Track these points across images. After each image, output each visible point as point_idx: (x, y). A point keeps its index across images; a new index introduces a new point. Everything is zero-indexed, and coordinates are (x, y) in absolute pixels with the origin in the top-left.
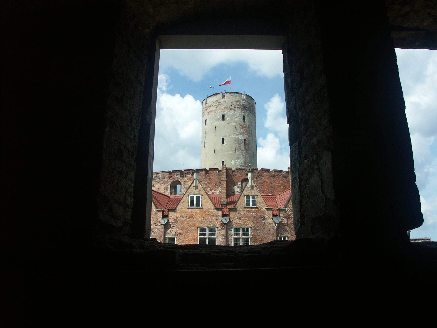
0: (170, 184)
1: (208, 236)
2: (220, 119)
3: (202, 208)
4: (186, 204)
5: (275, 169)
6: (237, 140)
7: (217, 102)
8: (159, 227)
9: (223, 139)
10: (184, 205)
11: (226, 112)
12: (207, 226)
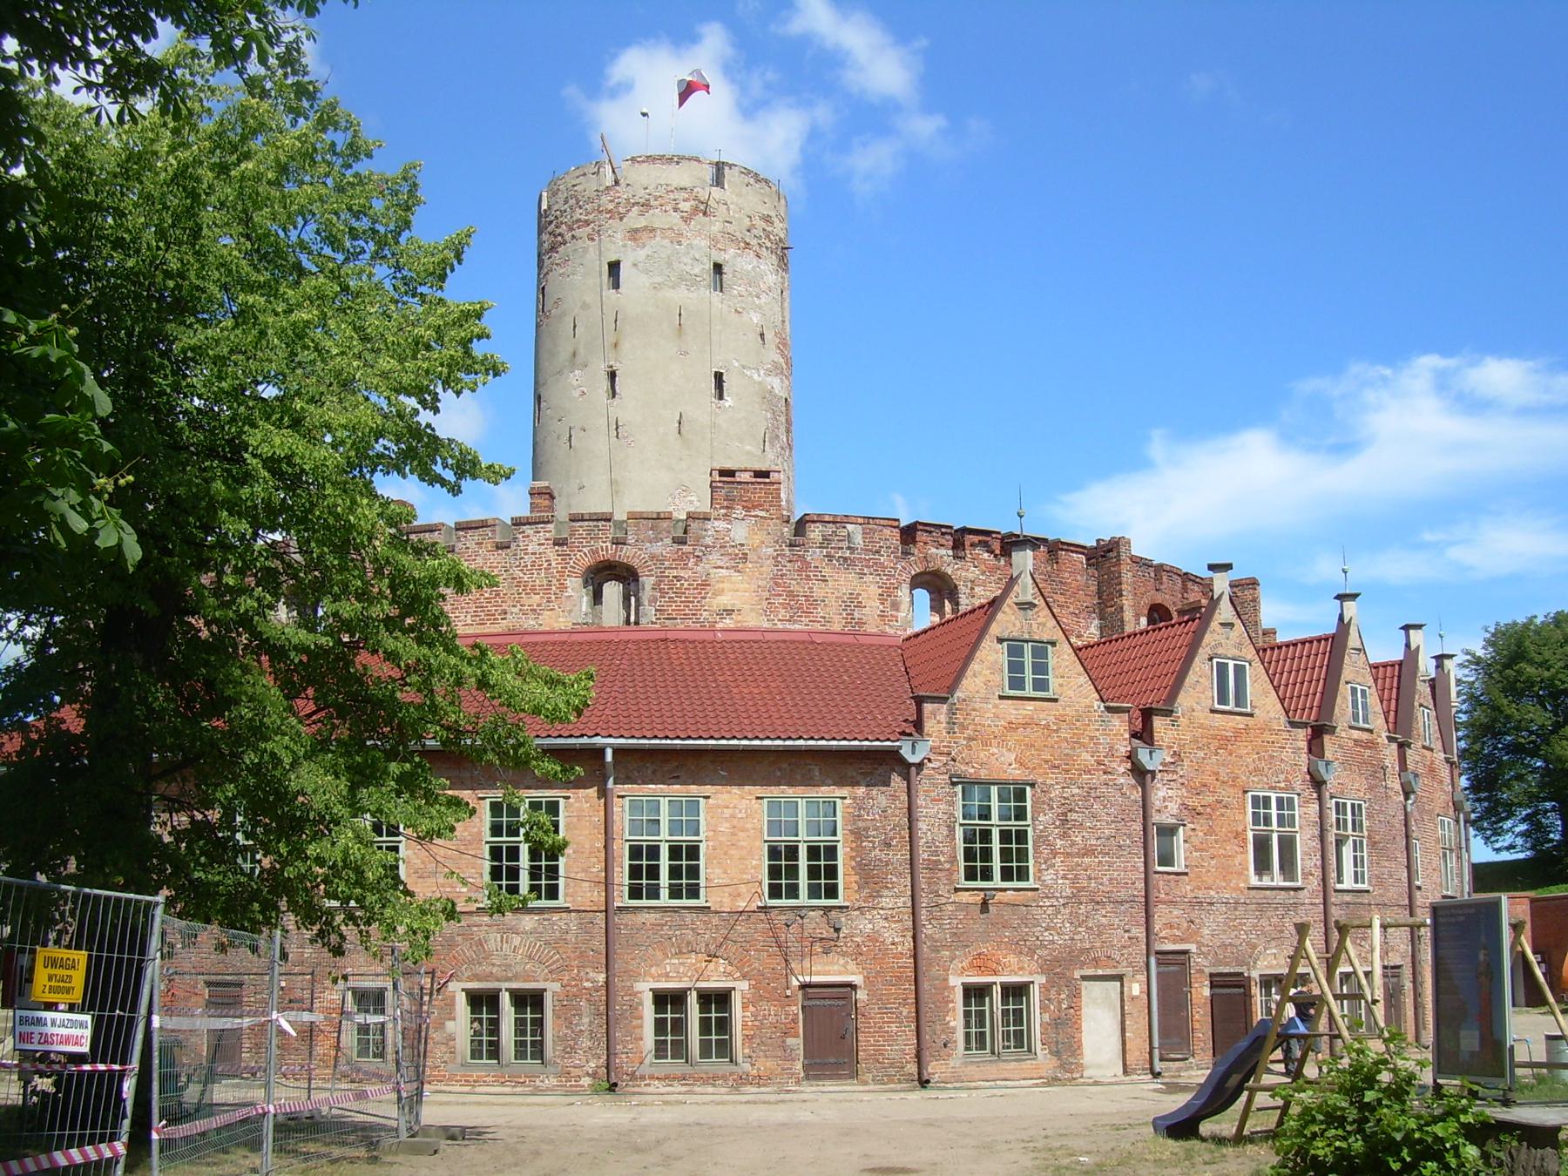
3: (1251, 715)
6: (767, 397)
8: (1122, 781)
9: (719, 377)
10: (1198, 697)
11: (728, 256)
12: (1274, 788)
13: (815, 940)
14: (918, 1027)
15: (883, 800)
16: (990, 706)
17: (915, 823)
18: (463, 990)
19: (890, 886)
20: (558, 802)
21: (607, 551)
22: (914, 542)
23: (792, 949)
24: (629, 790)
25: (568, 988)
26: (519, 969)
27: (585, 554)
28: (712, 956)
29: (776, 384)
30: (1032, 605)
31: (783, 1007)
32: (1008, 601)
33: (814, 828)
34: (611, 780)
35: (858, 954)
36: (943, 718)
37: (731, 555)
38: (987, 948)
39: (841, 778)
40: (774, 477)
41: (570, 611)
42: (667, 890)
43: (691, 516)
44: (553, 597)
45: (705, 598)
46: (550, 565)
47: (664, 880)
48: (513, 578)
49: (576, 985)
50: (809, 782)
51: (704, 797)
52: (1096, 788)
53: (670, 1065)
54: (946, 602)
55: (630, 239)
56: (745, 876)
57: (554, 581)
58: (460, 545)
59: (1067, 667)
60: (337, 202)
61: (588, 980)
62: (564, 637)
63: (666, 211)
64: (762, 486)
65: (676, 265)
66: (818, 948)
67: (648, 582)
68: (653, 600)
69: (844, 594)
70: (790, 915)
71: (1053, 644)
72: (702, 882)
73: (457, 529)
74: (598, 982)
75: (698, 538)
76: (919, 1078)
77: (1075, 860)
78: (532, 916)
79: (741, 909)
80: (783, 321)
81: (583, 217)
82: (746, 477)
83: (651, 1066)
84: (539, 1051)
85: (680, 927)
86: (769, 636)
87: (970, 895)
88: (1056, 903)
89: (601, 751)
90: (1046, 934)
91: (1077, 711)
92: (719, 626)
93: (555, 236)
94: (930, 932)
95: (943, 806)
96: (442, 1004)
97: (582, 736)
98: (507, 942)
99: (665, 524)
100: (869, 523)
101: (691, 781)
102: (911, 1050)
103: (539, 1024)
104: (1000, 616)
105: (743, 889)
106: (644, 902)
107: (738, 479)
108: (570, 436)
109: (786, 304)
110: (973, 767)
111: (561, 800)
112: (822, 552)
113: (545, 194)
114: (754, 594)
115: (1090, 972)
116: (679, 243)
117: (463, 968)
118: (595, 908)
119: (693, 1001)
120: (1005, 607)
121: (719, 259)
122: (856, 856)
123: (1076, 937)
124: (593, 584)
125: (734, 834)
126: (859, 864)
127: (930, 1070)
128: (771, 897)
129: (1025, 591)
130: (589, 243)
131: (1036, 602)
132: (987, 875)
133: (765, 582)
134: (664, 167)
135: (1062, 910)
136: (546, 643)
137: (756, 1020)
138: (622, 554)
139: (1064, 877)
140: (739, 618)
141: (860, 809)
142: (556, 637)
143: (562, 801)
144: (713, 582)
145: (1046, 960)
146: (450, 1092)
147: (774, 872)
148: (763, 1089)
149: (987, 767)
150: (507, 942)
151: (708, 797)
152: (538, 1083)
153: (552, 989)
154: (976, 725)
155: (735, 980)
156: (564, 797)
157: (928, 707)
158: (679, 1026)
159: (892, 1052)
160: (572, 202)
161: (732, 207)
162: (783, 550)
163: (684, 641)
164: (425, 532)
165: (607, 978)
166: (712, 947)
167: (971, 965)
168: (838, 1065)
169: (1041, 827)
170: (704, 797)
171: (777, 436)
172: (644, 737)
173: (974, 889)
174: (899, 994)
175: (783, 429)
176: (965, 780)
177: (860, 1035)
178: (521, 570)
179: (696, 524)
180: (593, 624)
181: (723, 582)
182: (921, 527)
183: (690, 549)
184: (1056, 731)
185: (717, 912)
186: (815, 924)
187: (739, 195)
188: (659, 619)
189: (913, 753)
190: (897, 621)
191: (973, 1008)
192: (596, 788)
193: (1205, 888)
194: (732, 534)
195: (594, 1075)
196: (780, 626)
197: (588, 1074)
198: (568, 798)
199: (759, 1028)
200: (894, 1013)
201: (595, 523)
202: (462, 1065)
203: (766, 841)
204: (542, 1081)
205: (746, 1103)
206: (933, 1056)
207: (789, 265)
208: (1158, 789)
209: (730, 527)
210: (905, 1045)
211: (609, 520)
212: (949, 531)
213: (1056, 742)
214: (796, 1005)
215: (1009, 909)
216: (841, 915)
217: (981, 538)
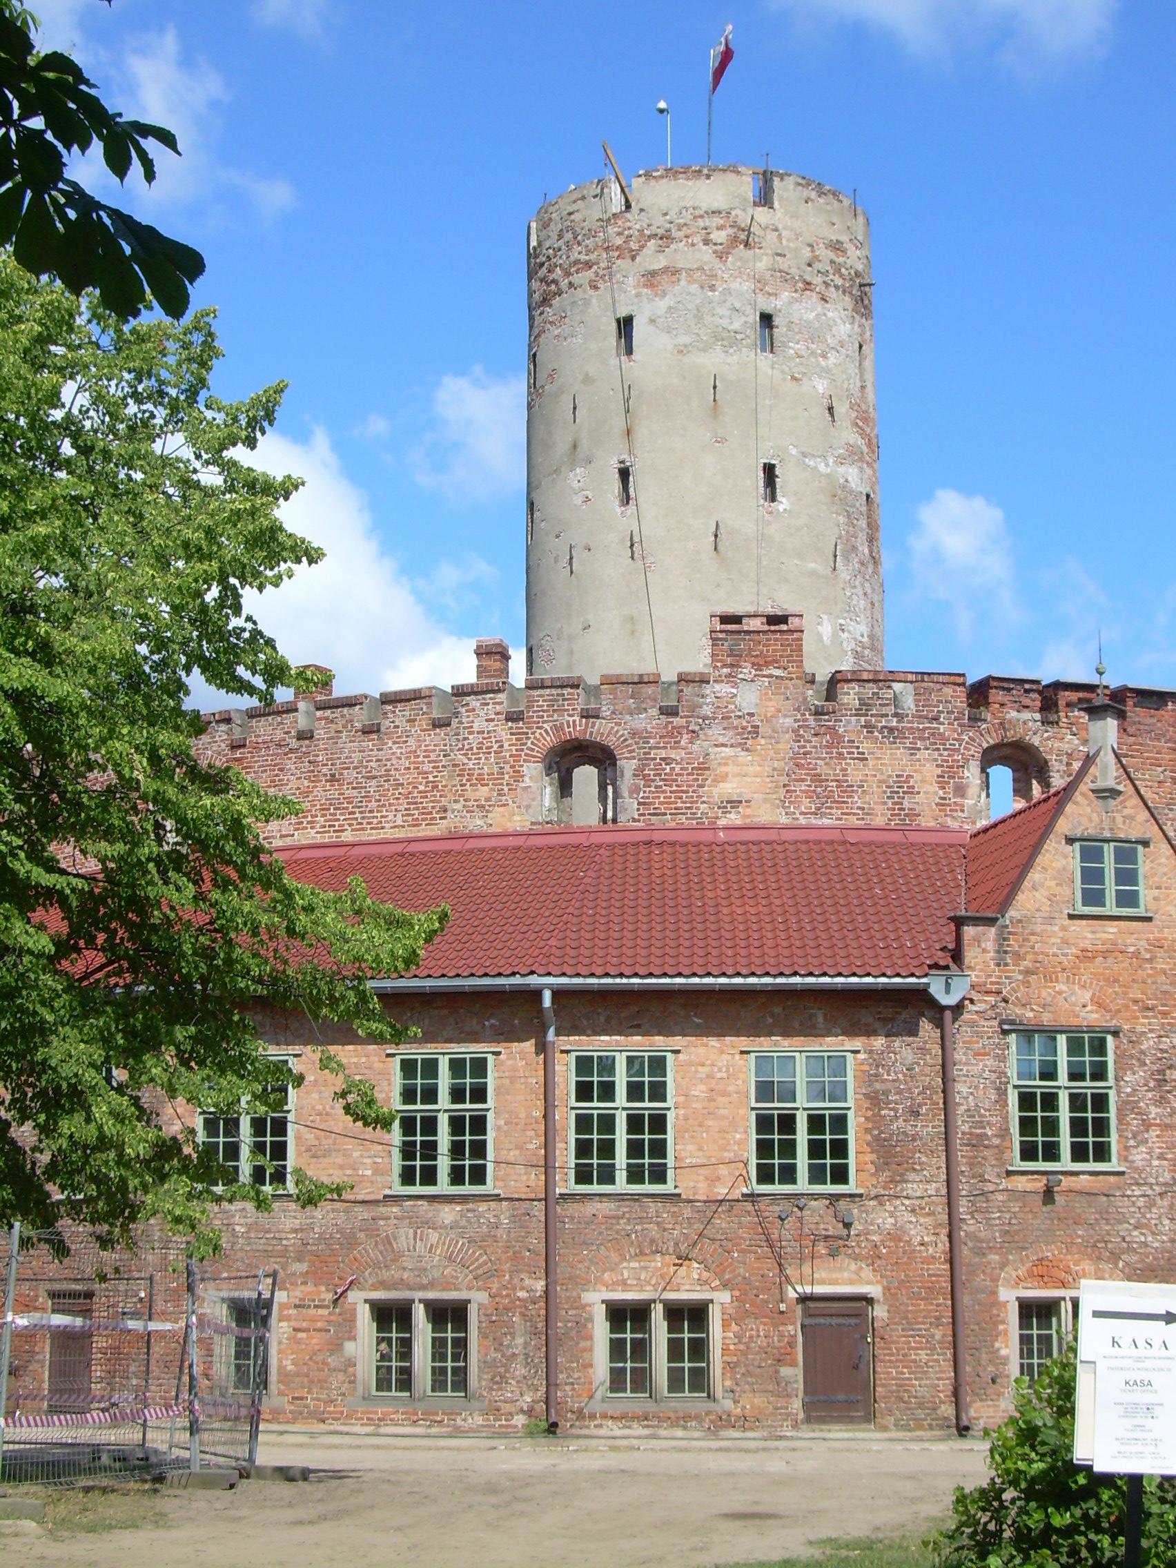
0: (978, 756)
6: (838, 494)
7: (721, 222)
9: (770, 472)
11: (781, 302)
13: (816, 1239)
14: (955, 1355)
15: (908, 1055)
16: (1056, 928)
17: (950, 1083)
18: (366, 1301)
19: (918, 1167)
20: (485, 1059)
21: (575, 727)
22: (987, 704)
23: (789, 1250)
24: (575, 1042)
25: (497, 1299)
28: (684, 1258)
29: (853, 476)
30: (1114, 793)
31: (775, 1325)
32: (1083, 788)
33: (818, 1092)
34: (552, 1031)
36: (990, 945)
37: (736, 728)
38: (1051, 1251)
40: (794, 623)
41: (528, 807)
42: (624, 1173)
43: (684, 679)
44: (506, 789)
45: (702, 786)
46: (502, 746)
47: (621, 1159)
48: (454, 765)
49: (508, 1295)
50: (809, 1030)
51: (673, 1052)
53: (629, 1400)
54: (1034, 782)
55: (646, 286)
56: (726, 1154)
57: (507, 768)
58: (386, 723)
59: (1165, 874)
60: (110, 367)
61: (522, 1289)
62: (519, 841)
63: (693, 245)
64: (778, 636)
65: (708, 319)
66: (822, 1249)
67: (627, 766)
68: (635, 790)
69: (890, 776)
70: (785, 1206)
71: (1146, 843)
72: (670, 1161)
73: (383, 703)
74: (536, 1291)
75: (693, 708)
76: (958, 1424)
78: (453, 1206)
79: (720, 1198)
80: (863, 387)
81: (583, 257)
82: (756, 624)
83: (603, 1401)
84: (461, 1382)
86: (787, 835)
87: (1028, 1181)
88: (1149, 1192)
89: (537, 994)
90: (1135, 1233)
92: (722, 822)
93: (548, 284)
94: (972, 1229)
95: (990, 1062)
96: (340, 1319)
97: (513, 974)
98: (421, 1240)
99: (650, 690)
100: (923, 681)
101: (655, 1031)
102: (946, 1385)
103: (461, 1345)
104: (1069, 808)
105: (723, 1171)
106: (595, 1188)
107: (746, 628)
108: (571, 558)
109: (868, 364)
110: (1032, 1010)
111: (490, 1057)
112: (858, 721)
113: (534, 225)
114: (768, 780)
117: (367, 1273)
118: (533, 1196)
119: (658, 1315)
120: (1077, 797)
121: (768, 305)
124: (559, 771)
125: (711, 1100)
126: (877, 1138)
127: (972, 1413)
129: (1104, 774)
130: (592, 292)
131: (1121, 788)
132: (1051, 1153)
133: (782, 763)
134: (690, 183)
135: (1159, 1202)
136: (494, 849)
137: (740, 1342)
138: (595, 731)
139: (1161, 1157)
140: (748, 811)
141: (877, 1066)
142: (511, 842)
143: (490, 1058)
144: (713, 764)
145: (1135, 1269)
146: (347, 1434)
147: (764, 1148)
148: (749, 1434)
149: (1051, 1009)
150: (421, 1240)
151: (677, 1052)
152: (459, 1422)
153: (478, 1299)
154: (1036, 953)
156: (493, 1053)
157: (969, 931)
158: (641, 1349)
159: (920, 1387)
160: (568, 236)
161: (784, 233)
162: (806, 720)
163: (673, 844)
164: (343, 706)
165: (547, 1286)
166: (683, 1247)
167: (1031, 1274)
168: (850, 1404)
169: (1129, 1090)
170: (673, 1052)
171: (854, 548)
172: (593, 975)
173: (1033, 1173)
174: (931, 1311)
175: (862, 537)
176: (1021, 1028)
177: (878, 1364)
178: (465, 755)
179: (690, 689)
180: (559, 822)
181: (726, 764)
182: (995, 684)
184: (1150, 960)
185: (690, 1201)
186: (818, 1216)
187: (795, 216)
188: (643, 815)
189: (948, 991)
190: (962, 811)
191: (1035, 1332)
192: (533, 1041)
194: (738, 700)
195: (530, 1412)
196: (803, 821)
197: (522, 1411)
198: (498, 1054)
199: (745, 1354)
200: (922, 1336)
201: (559, 691)
202: (364, 1398)
203: (753, 1109)
204: (465, 1420)
205: (717, 1450)
206: (977, 1395)
207: (873, 309)
209: (734, 691)
210: (938, 1379)
211: (577, 687)
212: (1034, 687)
213: (1149, 976)
214: (794, 1323)
215: (1084, 1199)
216: (852, 1206)
217: (1081, 695)
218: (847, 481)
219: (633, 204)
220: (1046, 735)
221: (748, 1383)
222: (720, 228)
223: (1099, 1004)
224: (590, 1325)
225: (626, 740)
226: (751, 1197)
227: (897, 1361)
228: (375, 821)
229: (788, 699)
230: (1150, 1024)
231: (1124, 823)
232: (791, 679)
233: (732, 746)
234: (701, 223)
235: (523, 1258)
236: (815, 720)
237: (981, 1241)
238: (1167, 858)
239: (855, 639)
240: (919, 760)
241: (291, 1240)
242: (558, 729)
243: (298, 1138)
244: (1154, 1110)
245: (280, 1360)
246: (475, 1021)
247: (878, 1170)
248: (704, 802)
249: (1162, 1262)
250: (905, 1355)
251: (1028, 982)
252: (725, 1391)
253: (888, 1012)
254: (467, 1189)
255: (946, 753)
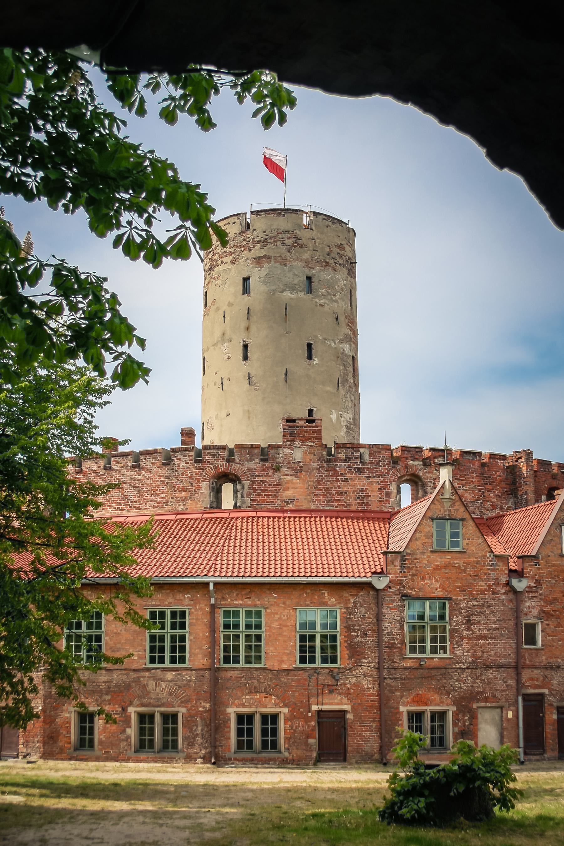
1: (525, 622)
2: (301, 289)
4: (555, 546)
5: (405, 445)
7: (289, 235)
8: (503, 597)
9: (309, 346)
10: (552, 549)
11: (315, 271)
16: (425, 557)
21: (223, 466)
26: (165, 700)
27: (211, 468)
35: (348, 694)
36: (398, 563)
39: (339, 597)
44: (194, 493)
52: (487, 602)
57: (194, 484)
59: (471, 534)
61: (201, 707)
68: (249, 494)
70: (311, 672)
71: (462, 520)
72: (263, 654)
75: (274, 458)
77: (475, 642)
82: (301, 423)
85: (251, 679)
89: (207, 584)
90: (457, 683)
91: (477, 558)
95: (397, 613)
98: (159, 686)
106: (231, 665)
110: (415, 591)
112: (345, 465)
115: (483, 704)
116: (285, 265)
122: (348, 640)
123: (475, 685)
128: (224, 662)
137: (291, 729)
140: (298, 504)
147: (302, 649)
155: (281, 707)
161: (318, 241)
162: (323, 464)
169: (455, 624)
171: (347, 380)
178: (176, 478)
183: (270, 465)
187: (322, 233)
190: (389, 504)
193: (555, 658)
194: (294, 456)
196: (321, 508)
197: (201, 758)
208: (526, 601)
210: (374, 744)
218: (344, 350)
219: (251, 227)
220: (425, 471)
221: (294, 745)
222: (289, 238)
223: (443, 588)
224: (229, 722)
225: (245, 472)
226: (297, 669)
227: (357, 736)
228: (137, 506)
229: (315, 455)
230: (464, 596)
231: (454, 512)
232: (317, 447)
233: (291, 475)
234: (280, 236)
235: (201, 694)
236: (327, 465)
237: (393, 687)
238: (472, 527)
239: (347, 421)
240: (371, 482)
241: (103, 686)
242: (216, 468)
243: (106, 643)
244: (465, 632)
245: (99, 736)
246: (181, 595)
247: (350, 657)
248: (278, 500)
249: (467, 695)
250: (360, 734)
251: (414, 579)
252: (285, 749)
253: (355, 592)
254: (178, 665)
255: (382, 479)
